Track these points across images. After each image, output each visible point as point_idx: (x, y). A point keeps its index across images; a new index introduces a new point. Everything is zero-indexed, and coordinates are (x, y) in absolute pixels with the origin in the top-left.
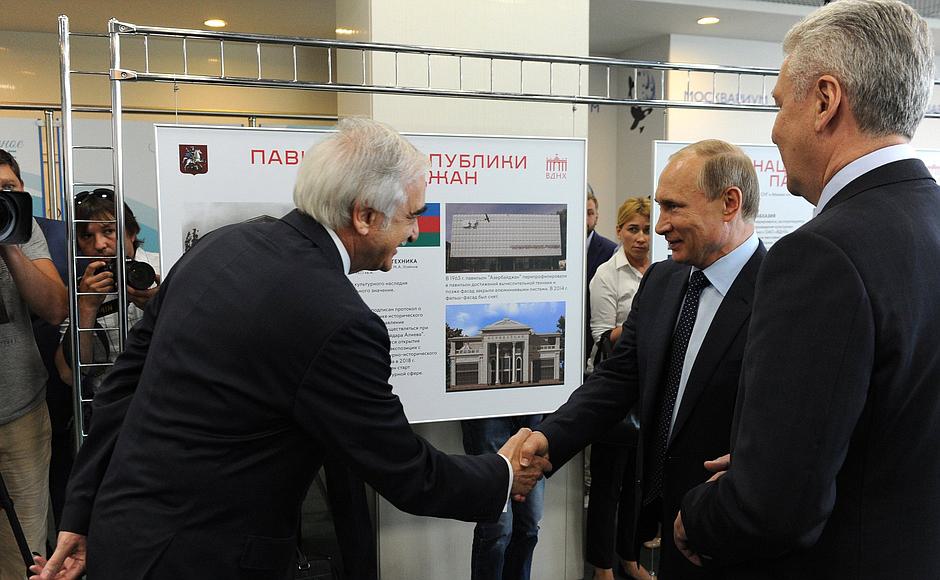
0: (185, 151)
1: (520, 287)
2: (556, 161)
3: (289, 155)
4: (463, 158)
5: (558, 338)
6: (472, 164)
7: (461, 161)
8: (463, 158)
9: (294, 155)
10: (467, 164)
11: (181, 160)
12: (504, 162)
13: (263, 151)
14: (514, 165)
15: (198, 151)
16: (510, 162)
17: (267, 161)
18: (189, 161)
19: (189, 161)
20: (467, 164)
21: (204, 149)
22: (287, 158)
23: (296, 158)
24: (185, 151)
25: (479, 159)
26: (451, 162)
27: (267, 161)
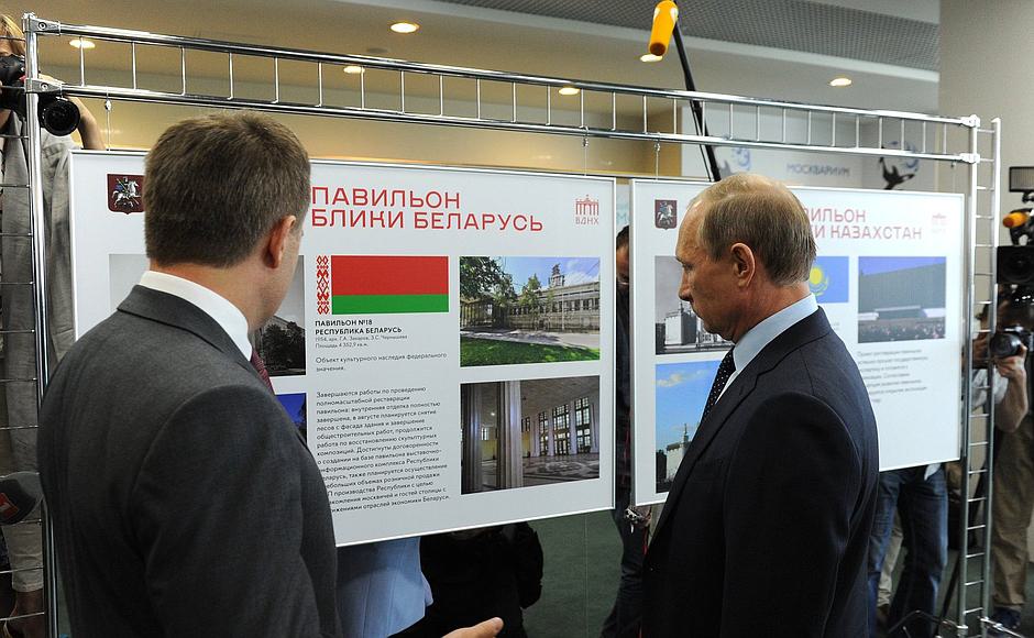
0: (660, 205)
1: (377, 502)
2: (587, 203)
3: (358, 193)
4: (317, 214)
5: (969, 547)
6: (329, 222)
7: (314, 217)
8: (317, 214)
9: (363, 194)
10: (322, 221)
11: (110, 194)
12: (372, 219)
13: (326, 189)
14: (386, 223)
15: (134, 183)
16: (381, 219)
17: (463, 225)
18: (121, 196)
19: (121, 196)
20: (322, 221)
21: (674, 203)
22: (355, 197)
23: (365, 197)
24: (660, 205)
25: (398, 197)
26: (505, 225)
27: (463, 225)
